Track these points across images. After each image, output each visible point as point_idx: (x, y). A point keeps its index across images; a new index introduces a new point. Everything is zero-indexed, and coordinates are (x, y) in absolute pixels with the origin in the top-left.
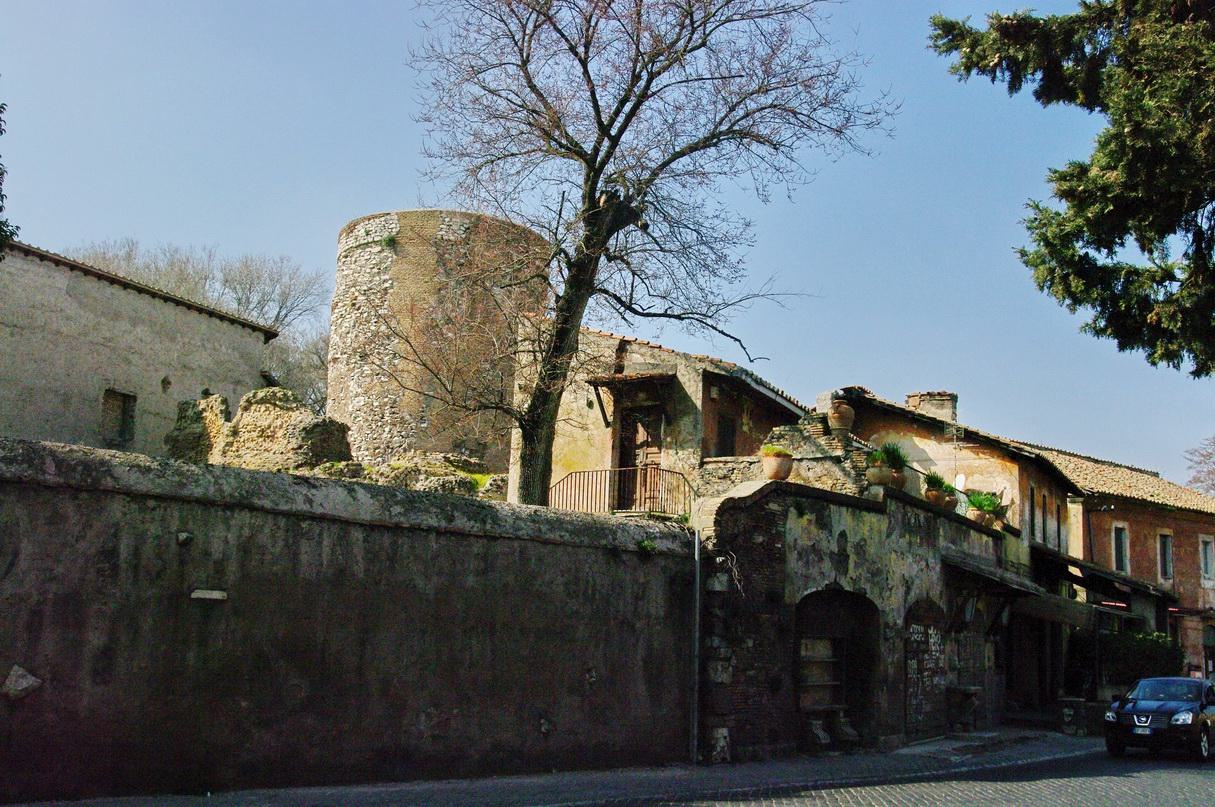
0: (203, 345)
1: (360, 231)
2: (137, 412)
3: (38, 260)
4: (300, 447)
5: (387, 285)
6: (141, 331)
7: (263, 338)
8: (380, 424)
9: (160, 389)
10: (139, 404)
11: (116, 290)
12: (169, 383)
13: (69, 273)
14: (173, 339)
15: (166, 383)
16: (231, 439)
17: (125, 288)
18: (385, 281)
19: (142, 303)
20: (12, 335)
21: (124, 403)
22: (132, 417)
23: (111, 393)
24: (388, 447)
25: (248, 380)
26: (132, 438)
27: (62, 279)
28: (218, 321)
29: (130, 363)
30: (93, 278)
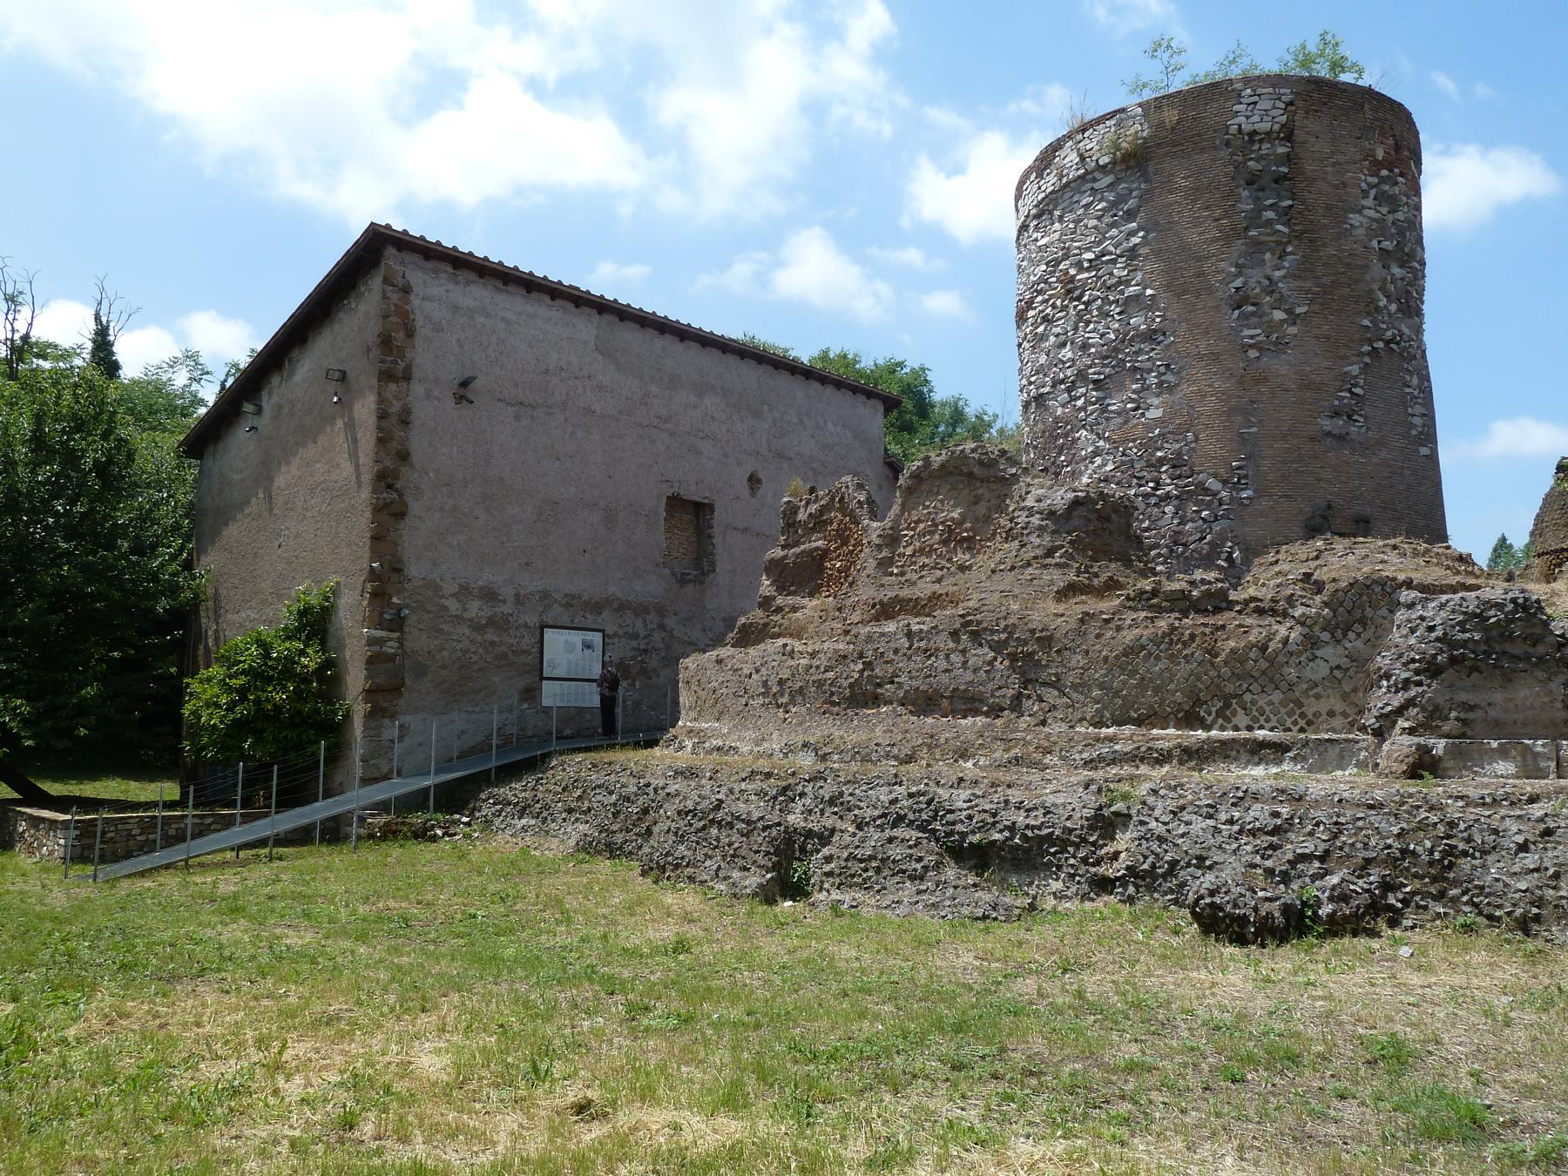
0: (801, 421)
1: (1069, 157)
2: (717, 531)
3: (547, 299)
4: (1050, 553)
5: (1135, 240)
6: (710, 402)
7: (881, 408)
8: (1153, 500)
9: (747, 491)
10: (719, 517)
11: (668, 342)
12: (759, 481)
13: (596, 318)
14: (758, 415)
15: (754, 481)
16: (885, 553)
17: (682, 340)
18: (1132, 233)
19: (709, 360)
20: (517, 418)
21: (697, 518)
22: (710, 537)
23: (675, 503)
24: (1176, 543)
25: (868, 471)
26: (713, 565)
27: (586, 327)
28: (817, 385)
29: (698, 453)
30: (633, 325)
